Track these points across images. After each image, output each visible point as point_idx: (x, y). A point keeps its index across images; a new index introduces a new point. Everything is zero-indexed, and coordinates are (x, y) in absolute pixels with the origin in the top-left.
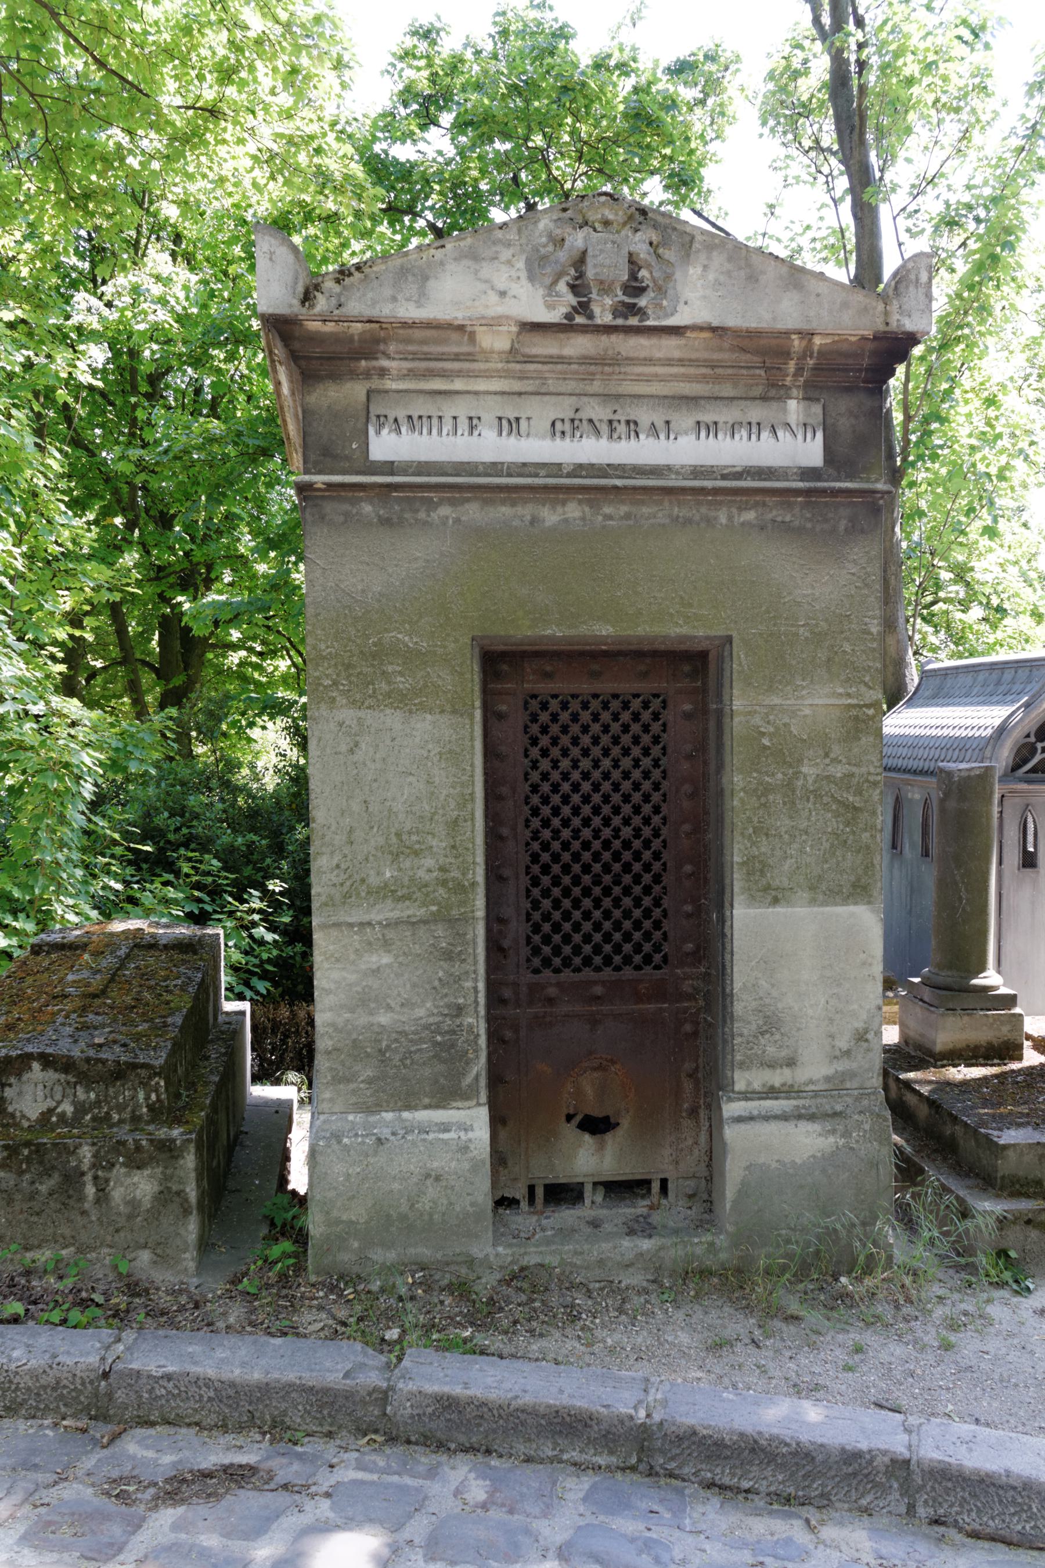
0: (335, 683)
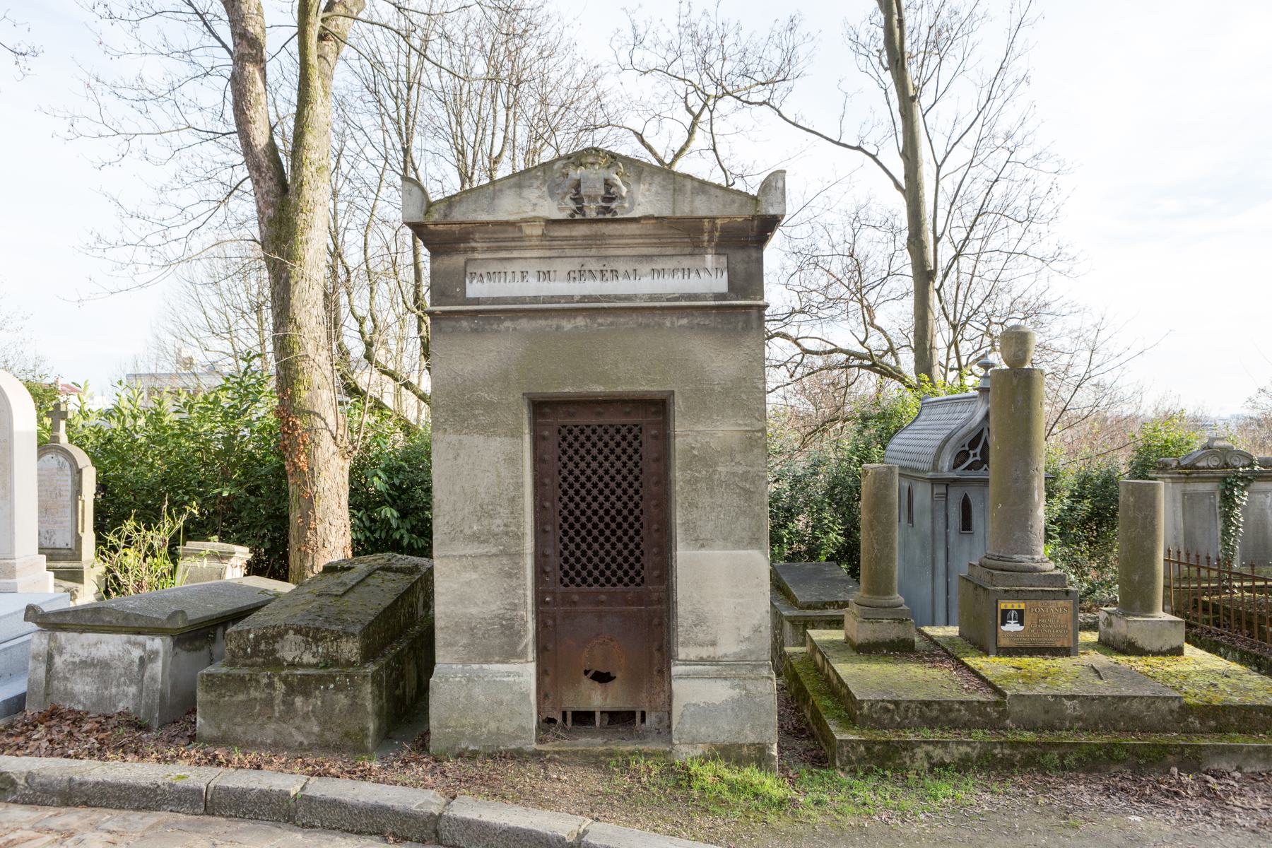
0: (446, 420)
